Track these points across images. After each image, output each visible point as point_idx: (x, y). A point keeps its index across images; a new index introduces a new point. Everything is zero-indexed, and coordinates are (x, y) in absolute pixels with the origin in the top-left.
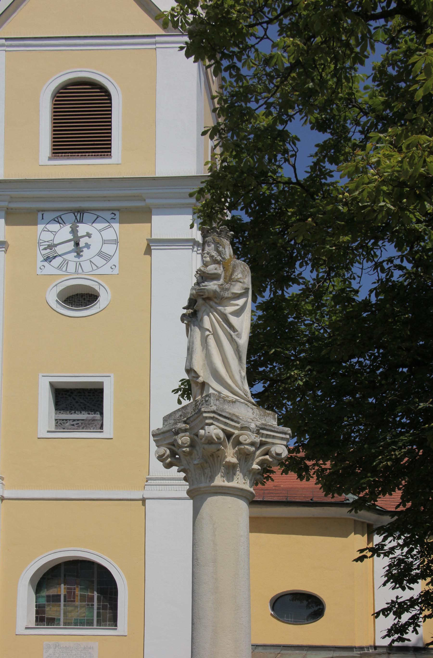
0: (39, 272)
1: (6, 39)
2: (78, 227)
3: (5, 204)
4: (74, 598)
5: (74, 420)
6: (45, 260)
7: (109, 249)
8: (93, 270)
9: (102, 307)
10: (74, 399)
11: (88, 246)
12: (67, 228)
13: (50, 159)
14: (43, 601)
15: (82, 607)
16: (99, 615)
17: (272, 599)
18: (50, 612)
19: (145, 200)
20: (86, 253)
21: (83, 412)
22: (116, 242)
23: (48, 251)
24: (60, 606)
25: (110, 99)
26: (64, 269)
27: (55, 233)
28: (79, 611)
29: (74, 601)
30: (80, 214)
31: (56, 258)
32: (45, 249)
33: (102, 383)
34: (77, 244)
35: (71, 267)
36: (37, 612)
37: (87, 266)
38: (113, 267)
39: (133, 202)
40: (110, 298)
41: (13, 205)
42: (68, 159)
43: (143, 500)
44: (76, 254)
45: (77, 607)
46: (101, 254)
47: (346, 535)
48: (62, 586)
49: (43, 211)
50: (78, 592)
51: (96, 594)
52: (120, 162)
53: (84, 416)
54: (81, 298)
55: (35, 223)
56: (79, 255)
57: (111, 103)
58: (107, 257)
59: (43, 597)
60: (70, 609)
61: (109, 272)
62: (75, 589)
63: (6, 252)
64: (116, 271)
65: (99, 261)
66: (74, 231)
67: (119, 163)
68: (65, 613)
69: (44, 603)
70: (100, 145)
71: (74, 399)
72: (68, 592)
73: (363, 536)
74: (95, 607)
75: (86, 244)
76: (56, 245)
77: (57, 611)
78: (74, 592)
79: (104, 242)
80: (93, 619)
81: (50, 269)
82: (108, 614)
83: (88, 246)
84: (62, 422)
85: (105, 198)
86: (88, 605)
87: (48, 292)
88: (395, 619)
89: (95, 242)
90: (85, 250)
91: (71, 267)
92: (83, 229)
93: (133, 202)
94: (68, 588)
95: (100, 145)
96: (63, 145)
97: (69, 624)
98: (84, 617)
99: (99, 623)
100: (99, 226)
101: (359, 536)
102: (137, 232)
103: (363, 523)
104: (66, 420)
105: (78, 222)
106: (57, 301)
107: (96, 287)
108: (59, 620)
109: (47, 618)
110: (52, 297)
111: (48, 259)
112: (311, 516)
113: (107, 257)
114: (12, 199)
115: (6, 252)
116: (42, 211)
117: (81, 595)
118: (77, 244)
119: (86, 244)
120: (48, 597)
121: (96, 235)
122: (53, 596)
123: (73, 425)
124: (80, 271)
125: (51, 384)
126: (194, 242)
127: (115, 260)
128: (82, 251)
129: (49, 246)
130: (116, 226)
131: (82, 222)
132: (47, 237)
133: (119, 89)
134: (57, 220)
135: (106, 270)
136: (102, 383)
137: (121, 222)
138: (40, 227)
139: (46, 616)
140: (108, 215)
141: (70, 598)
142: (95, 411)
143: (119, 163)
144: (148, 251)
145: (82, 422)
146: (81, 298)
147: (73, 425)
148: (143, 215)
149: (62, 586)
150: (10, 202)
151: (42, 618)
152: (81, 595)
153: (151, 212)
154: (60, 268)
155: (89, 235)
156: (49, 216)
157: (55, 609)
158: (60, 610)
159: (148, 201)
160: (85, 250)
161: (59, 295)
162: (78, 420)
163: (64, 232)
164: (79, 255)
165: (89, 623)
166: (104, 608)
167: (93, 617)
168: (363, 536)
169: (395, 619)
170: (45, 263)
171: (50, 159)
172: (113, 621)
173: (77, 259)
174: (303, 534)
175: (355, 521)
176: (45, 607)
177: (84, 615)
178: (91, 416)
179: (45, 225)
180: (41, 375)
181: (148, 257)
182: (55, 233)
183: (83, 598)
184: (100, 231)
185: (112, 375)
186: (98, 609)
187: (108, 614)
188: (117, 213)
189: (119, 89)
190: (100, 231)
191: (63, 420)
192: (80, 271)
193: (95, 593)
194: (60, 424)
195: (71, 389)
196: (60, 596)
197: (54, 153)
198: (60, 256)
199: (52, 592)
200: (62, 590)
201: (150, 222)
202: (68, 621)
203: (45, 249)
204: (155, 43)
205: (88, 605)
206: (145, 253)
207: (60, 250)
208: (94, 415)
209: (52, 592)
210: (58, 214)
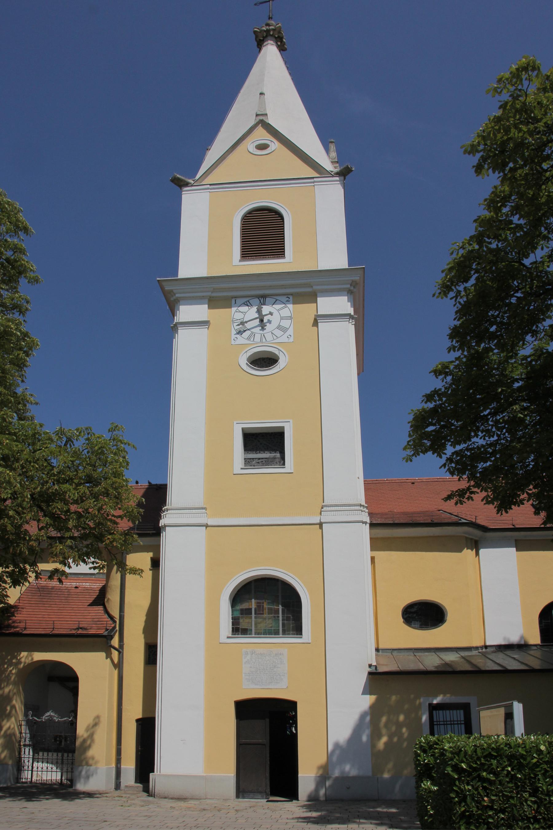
0: (233, 342)
1: (210, 185)
2: (262, 308)
3: (209, 294)
4: (263, 611)
5: (259, 459)
6: (238, 333)
7: (286, 323)
8: (274, 339)
9: (282, 367)
10: (259, 441)
11: (269, 322)
12: (255, 309)
13: (240, 261)
14: (237, 614)
15: (269, 619)
16: (283, 625)
19: (312, 287)
20: (269, 327)
21: (266, 452)
22: (291, 318)
23: (241, 326)
24: (251, 618)
25: (283, 221)
26: (252, 339)
27: (245, 313)
28: (267, 622)
29: (263, 614)
30: (263, 299)
31: (246, 332)
32: (238, 325)
33: (283, 427)
34: (262, 321)
35: (257, 338)
36: (233, 624)
37: (269, 337)
38: (289, 337)
39: (303, 288)
40: (287, 360)
41: (214, 295)
42: (254, 260)
43: (321, 525)
44: (260, 328)
45: (265, 619)
46: (279, 327)
47: (460, 551)
48: (253, 600)
49: (236, 297)
50: (266, 606)
51: (280, 607)
52: (292, 261)
53: (266, 455)
54: (264, 361)
55: (230, 307)
56: (263, 329)
57: (284, 224)
58: (284, 330)
59: (237, 610)
60: (260, 620)
61: (286, 340)
62: (263, 603)
63: (208, 328)
64: (291, 340)
65: (278, 333)
66: (259, 311)
67: (291, 261)
68: (256, 624)
69: (238, 615)
70: (278, 250)
71: (259, 441)
72: (258, 606)
73: (472, 550)
74: (281, 618)
75: (268, 320)
76: (246, 322)
77: (248, 623)
78: (263, 606)
79: (282, 318)
80: (279, 630)
81: (241, 340)
82: (291, 624)
83: (269, 322)
84: (249, 460)
86: (274, 617)
87: (240, 357)
89: (275, 319)
90: (268, 324)
91: (257, 338)
92: (266, 309)
93: (303, 288)
94: (258, 603)
95: (278, 250)
96: (249, 251)
97: (258, 634)
98: (272, 627)
99: (284, 632)
101: (469, 551)
102: (307, 310)
103: (471, 539)
104: (253, 459)
105: (262, 305)
106: (247, 364)
107: (277, 352)
108: (251, 630)
109: (241, 629)
110: (243, 361)
111: (240, 333)
112: (432, 535)
113: (284, 330)
114: (214, 290)
115: (208, 328)
116: (235, 298)
117: (269, 609)
118: (262, 321)
119: (268, 320)
120: (242, 610)
121: (275, 313)
122: (246, 609)
123: (258, 463)
124: (264, 340)
125: (243, 429)
126: (349, 315)
127: (291, 332)
128: (266, 326)
129: (241, 323)
130: (290, 306)
131: (265, 305)
132: (239, 316)
133: (289, 212)
134: (246, 304)
135: (284, 339)
136: (283, 427)
137: (294, 303)
138: (234, 309)
139: (240, 627)
140: (284, 299)
141: (259, 610)
142: (275, 451)
143: (291, 261)
144: (315, 323)
145: (266, 460)
146: (264, 361)
147: (258, 463)
148: (312, 297)
149: (253, 600)
150: (212, 292)
151: (238, 629)
152: (269, 609)
153: (317, 295)
154: (249, 339)
155: (271, 314)
156: (239, 301)
157: (247, 620)
158: (252, 621)
159: (315, 287)
160: (268, 324)
161: (248, 360)
162: (262, 458)
163: (251, 312)
164: (263, 329)
165: (276, 633)
166: (288, 619)
167: (279, 627)
168: (472, 550)
170: (238, 336)
171: (240, 261)
172: (298, 630)
173: (261, 332)
174: (544, 550)
175: (466, 538)
176: (239, 619)
177: (271, 625)
178: (273, 455)
179: (236, 308)
180: (235, 422)
181: (315, 328)
182: (245, 313)
183: (270, 611)
184: (278, 310)
185: (291, 421)
186: (283, 620)
187: (295, 626)
188: (291, 297)
189: (289, 212)
190: (278, 310)
191: (250, 459)
192: (264, 340)
193: (280, 606)
194: (248, 462)
195: (256, 434)
196: (251, 609)
197: (243, 257)
198: (249, 330)
199: (245, 606)
200: (253, 604)
201: (316, 302)
202: (258, 631)
203: (238, 325)
204: (314, 182)
205: (274, 617)
206: (313, 325)
207: (248, 326)
208: (275, 454)
209: (245, 606)
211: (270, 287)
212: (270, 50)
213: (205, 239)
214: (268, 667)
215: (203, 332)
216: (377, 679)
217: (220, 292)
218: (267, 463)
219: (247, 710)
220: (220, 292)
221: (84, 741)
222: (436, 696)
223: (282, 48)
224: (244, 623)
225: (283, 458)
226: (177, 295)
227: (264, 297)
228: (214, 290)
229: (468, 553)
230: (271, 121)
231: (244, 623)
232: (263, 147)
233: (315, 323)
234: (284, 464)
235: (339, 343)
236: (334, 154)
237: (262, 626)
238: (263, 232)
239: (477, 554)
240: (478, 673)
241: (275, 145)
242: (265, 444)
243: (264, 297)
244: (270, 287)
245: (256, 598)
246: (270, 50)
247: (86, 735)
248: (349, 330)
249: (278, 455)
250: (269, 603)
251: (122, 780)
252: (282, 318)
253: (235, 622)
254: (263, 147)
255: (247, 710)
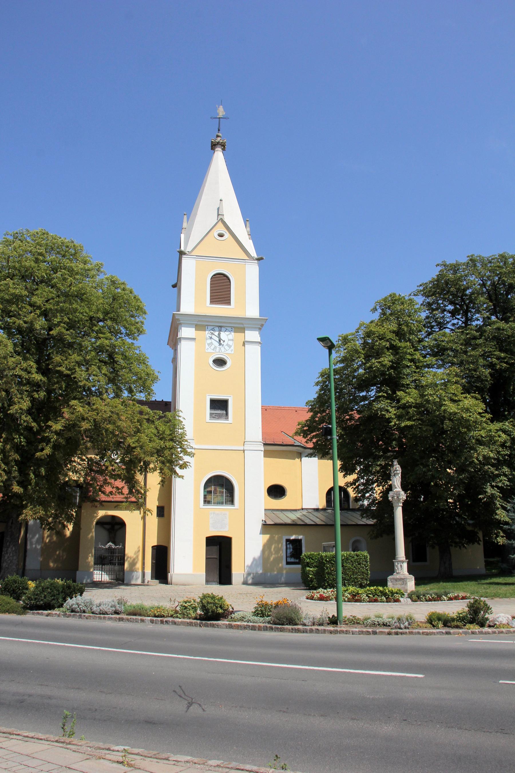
7: (231, 343)
17: (272, 498)
18: (208, 498)
22: (232, 340)
25: (230, 281)
28: (219, 499)
39: (239, 325)
41: (198, 323)
43: (244, 451)
46: (227, 345)
50: (218, 490)
53: (219, 412)
54: (220, 362)
58: (230, 346)
64: (233, 352)
79: (229, 340)
82: (229, 499)
85: (230, 323)
88: (140, 514)
92: (222, 334)
93: (239, 325)
99: (226, 504)
100: (227, 333)
102: (240, 336)
107: (226, 358)
113: (230, 346)
114: (199, 321)
127: (232, 348)
130: (233, 333)
138: (207, 332)
139: (207, 500)
140: (230, 329)
142: (223, 410)
144: (244, 345)
146: (220, 362)
151: (207, 502)
154: (213, 350)
156: (210, 328)
157: (210, 496)
159: (245, 325)
165: (222, 503)
166: (227, 496)
169: (140, 514)
172: (232, 502)
183: (220, 492)
187: (231, 500)
190: (227, 335)
199: (209, 489)
210: (213, 327)
211: (225, 323)
212: (219, 155)
213: (194, 297)
214: (220, 520)
215: (192, 344)
216: (266, 527)
217: (202, 323)
218: (219, 417)
219: (211, 541)
220: (202, 323)
221: (134, 559)
222: (292, 535)
223: (224, 150)
224: (208, 498)
225: (227, 414)
226: (181, 322)
227: (220, 327)
228: (199, 321)
229: (297, 460)
230: (226, 220)
231: (208, 499)
232: (221, 235)
233: (244, 345)
234: (228, 418)
235: (254, 355)
236: (249, 229)
237: (216, 500)
238: (221, 288)
239: (301, 460)
240: (306, 525)
241: (227, 235)
242: (219, 406)
243: (221, 327)
244: (225, 323)
245: (214, 485)
246: (219, 155)
247: (134, 556)
248: (258, 349)
249: (225, 412)
250: (220, 488)
251: (146, 577)
252: (229, 340)
253: (205, 496)
254: (221, 235)
255: (211, 541)
